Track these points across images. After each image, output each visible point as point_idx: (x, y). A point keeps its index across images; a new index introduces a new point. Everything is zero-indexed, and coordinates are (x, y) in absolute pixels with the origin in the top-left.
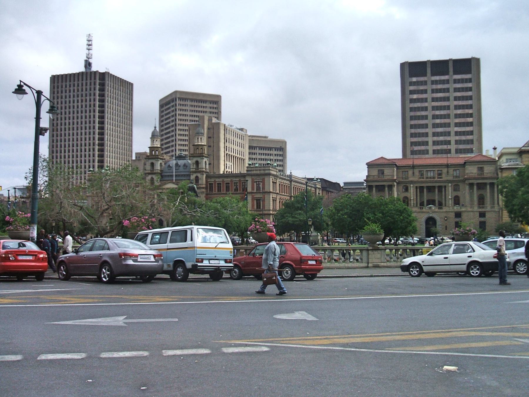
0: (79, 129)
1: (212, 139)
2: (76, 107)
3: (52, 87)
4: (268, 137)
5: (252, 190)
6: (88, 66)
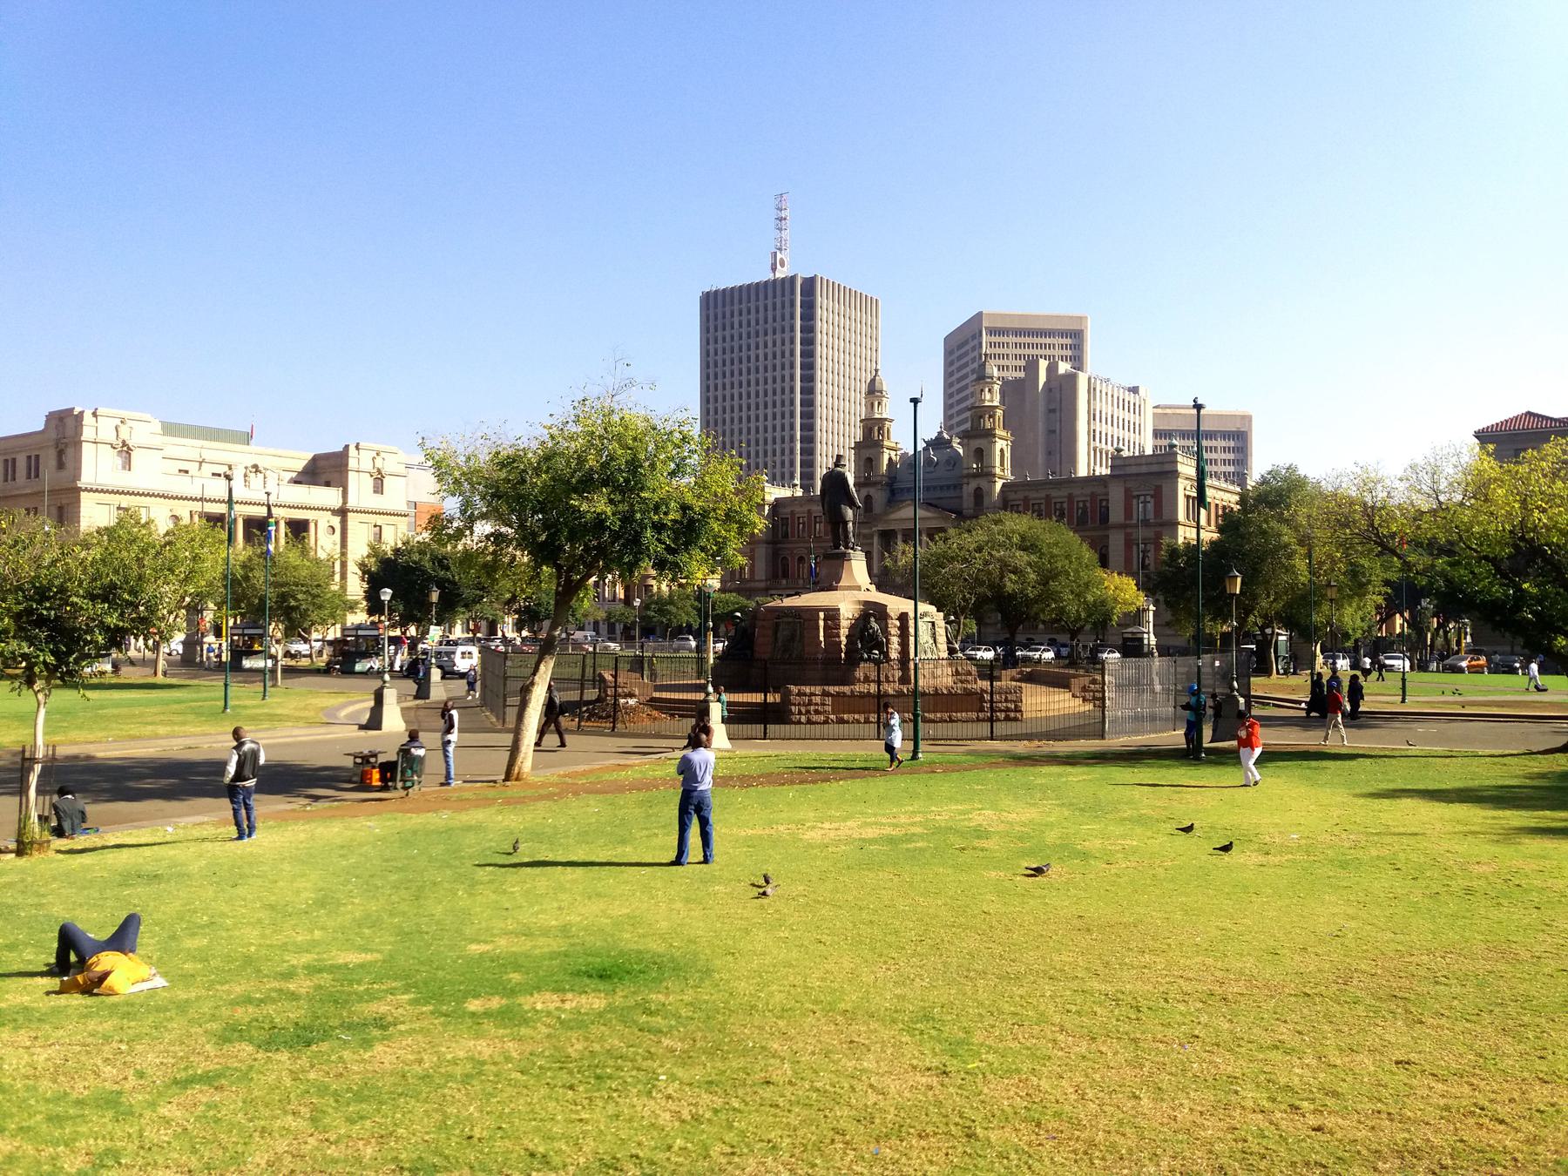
1: (1058, 414)
5: (1125, 519)
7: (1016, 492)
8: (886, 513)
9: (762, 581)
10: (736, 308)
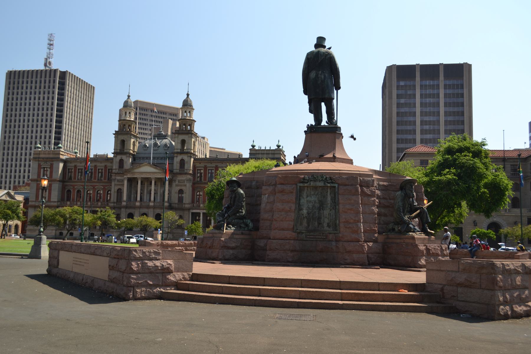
2: (35, 121)
3: (8, 83)
4: (225, 149)
7: (200, 163)
8: (133, 169)
9: (55, 202)
10: (25, 80)
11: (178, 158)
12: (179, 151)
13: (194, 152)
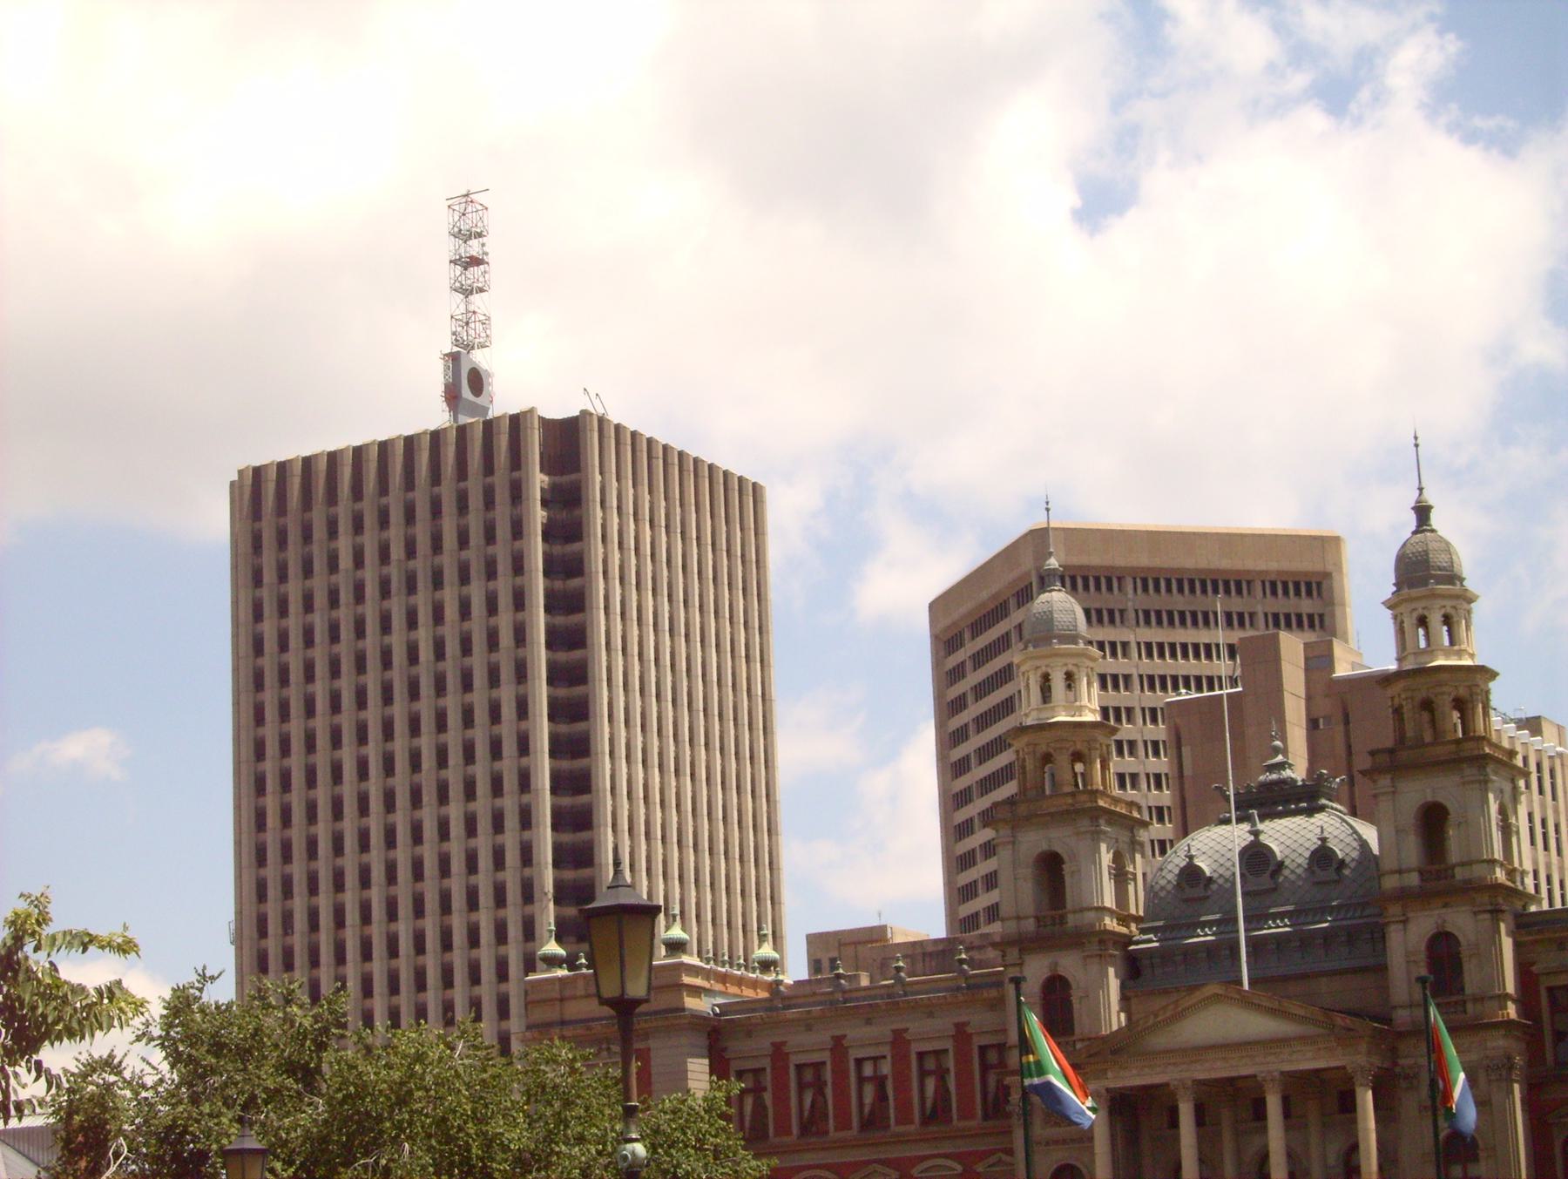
0: (429, 796)
6: (466, 393)
11: (1412, 927)
12: (1413, 880)
13: (1511, 873)
